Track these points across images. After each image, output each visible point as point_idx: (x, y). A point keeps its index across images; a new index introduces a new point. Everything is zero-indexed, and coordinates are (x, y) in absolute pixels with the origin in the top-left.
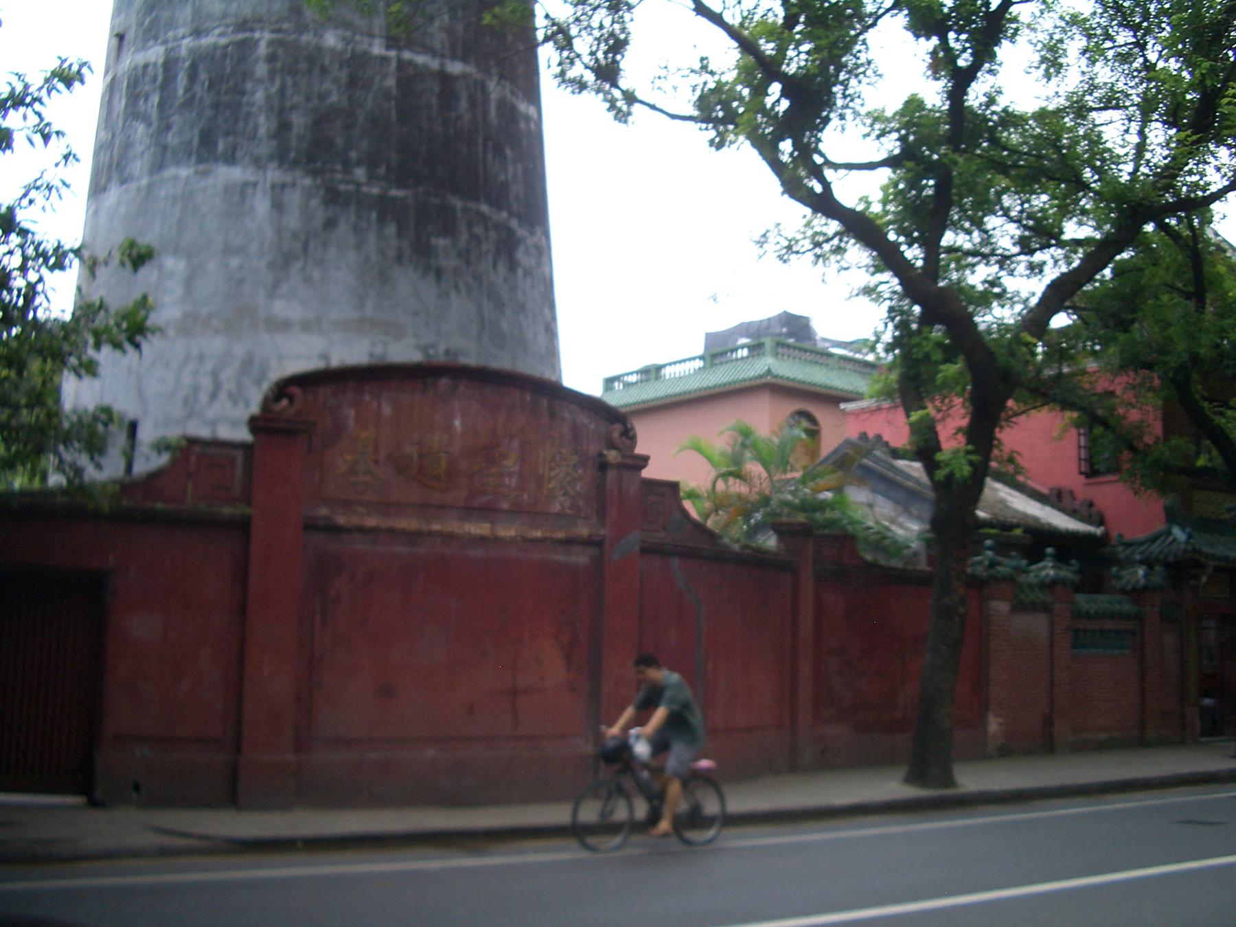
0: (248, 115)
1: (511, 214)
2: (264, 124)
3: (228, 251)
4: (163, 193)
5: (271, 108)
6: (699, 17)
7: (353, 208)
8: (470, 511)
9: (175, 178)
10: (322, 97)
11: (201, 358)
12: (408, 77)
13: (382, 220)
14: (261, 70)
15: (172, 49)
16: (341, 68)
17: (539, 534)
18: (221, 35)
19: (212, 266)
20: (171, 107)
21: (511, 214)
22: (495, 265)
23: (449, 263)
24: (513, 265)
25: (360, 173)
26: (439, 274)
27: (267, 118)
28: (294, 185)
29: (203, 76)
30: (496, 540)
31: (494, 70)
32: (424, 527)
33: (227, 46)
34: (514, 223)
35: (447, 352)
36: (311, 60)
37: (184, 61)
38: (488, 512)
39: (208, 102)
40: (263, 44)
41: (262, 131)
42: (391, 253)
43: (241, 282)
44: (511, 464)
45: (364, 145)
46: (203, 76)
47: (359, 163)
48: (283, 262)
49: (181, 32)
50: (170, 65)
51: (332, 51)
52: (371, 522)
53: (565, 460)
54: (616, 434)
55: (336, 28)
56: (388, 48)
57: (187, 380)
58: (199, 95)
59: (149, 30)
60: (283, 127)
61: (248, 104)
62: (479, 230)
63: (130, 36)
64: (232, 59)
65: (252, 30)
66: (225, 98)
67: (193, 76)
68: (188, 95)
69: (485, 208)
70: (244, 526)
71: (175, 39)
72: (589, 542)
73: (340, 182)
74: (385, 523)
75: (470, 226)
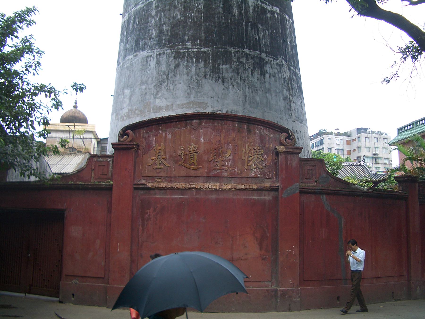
1: (261, 51)
2: (154, 32)
3: (142, 83)
4: (125, 66)
5: (157, 26)
8: (208, 178)
9: (129, 59)
10: (174, 18)
13: (198, 61)
14: (154, 13)
16: (181, 5)
17: (243, 187)
18: (142, 3)
19: (137, 90)
22: (252, 74)
23: (228, 75)
24: (263, 73)
25: (189, 44)
26: (223, 81)
27: (155, 30)
29: (137, 20)
30: (223, 190)
32: (187, 186)
33: (143, 7)
34: (264, 55)
35: (227, 112)
37: (132, 17)
38: (217, 178)
39: (138, 29)
41: (153, 35)
42: (202, 74)
43: (146, 94)
44: (229, 155)
45: (190, 33)
46: (137, 20)
48: (159, 84)
52: (162, 185)
53: (256, 152)
54: (283, 138)
60: (161, 32)
62: (244, 60)
66: (142, 26)
67: (134, 22)
68: (133, 28)
69: (247, 51)
70: (109, 189)
71: (131, 10)
72: (270, 189)
73: (181, 49)
74: (169, 185)
75: (239, 58)
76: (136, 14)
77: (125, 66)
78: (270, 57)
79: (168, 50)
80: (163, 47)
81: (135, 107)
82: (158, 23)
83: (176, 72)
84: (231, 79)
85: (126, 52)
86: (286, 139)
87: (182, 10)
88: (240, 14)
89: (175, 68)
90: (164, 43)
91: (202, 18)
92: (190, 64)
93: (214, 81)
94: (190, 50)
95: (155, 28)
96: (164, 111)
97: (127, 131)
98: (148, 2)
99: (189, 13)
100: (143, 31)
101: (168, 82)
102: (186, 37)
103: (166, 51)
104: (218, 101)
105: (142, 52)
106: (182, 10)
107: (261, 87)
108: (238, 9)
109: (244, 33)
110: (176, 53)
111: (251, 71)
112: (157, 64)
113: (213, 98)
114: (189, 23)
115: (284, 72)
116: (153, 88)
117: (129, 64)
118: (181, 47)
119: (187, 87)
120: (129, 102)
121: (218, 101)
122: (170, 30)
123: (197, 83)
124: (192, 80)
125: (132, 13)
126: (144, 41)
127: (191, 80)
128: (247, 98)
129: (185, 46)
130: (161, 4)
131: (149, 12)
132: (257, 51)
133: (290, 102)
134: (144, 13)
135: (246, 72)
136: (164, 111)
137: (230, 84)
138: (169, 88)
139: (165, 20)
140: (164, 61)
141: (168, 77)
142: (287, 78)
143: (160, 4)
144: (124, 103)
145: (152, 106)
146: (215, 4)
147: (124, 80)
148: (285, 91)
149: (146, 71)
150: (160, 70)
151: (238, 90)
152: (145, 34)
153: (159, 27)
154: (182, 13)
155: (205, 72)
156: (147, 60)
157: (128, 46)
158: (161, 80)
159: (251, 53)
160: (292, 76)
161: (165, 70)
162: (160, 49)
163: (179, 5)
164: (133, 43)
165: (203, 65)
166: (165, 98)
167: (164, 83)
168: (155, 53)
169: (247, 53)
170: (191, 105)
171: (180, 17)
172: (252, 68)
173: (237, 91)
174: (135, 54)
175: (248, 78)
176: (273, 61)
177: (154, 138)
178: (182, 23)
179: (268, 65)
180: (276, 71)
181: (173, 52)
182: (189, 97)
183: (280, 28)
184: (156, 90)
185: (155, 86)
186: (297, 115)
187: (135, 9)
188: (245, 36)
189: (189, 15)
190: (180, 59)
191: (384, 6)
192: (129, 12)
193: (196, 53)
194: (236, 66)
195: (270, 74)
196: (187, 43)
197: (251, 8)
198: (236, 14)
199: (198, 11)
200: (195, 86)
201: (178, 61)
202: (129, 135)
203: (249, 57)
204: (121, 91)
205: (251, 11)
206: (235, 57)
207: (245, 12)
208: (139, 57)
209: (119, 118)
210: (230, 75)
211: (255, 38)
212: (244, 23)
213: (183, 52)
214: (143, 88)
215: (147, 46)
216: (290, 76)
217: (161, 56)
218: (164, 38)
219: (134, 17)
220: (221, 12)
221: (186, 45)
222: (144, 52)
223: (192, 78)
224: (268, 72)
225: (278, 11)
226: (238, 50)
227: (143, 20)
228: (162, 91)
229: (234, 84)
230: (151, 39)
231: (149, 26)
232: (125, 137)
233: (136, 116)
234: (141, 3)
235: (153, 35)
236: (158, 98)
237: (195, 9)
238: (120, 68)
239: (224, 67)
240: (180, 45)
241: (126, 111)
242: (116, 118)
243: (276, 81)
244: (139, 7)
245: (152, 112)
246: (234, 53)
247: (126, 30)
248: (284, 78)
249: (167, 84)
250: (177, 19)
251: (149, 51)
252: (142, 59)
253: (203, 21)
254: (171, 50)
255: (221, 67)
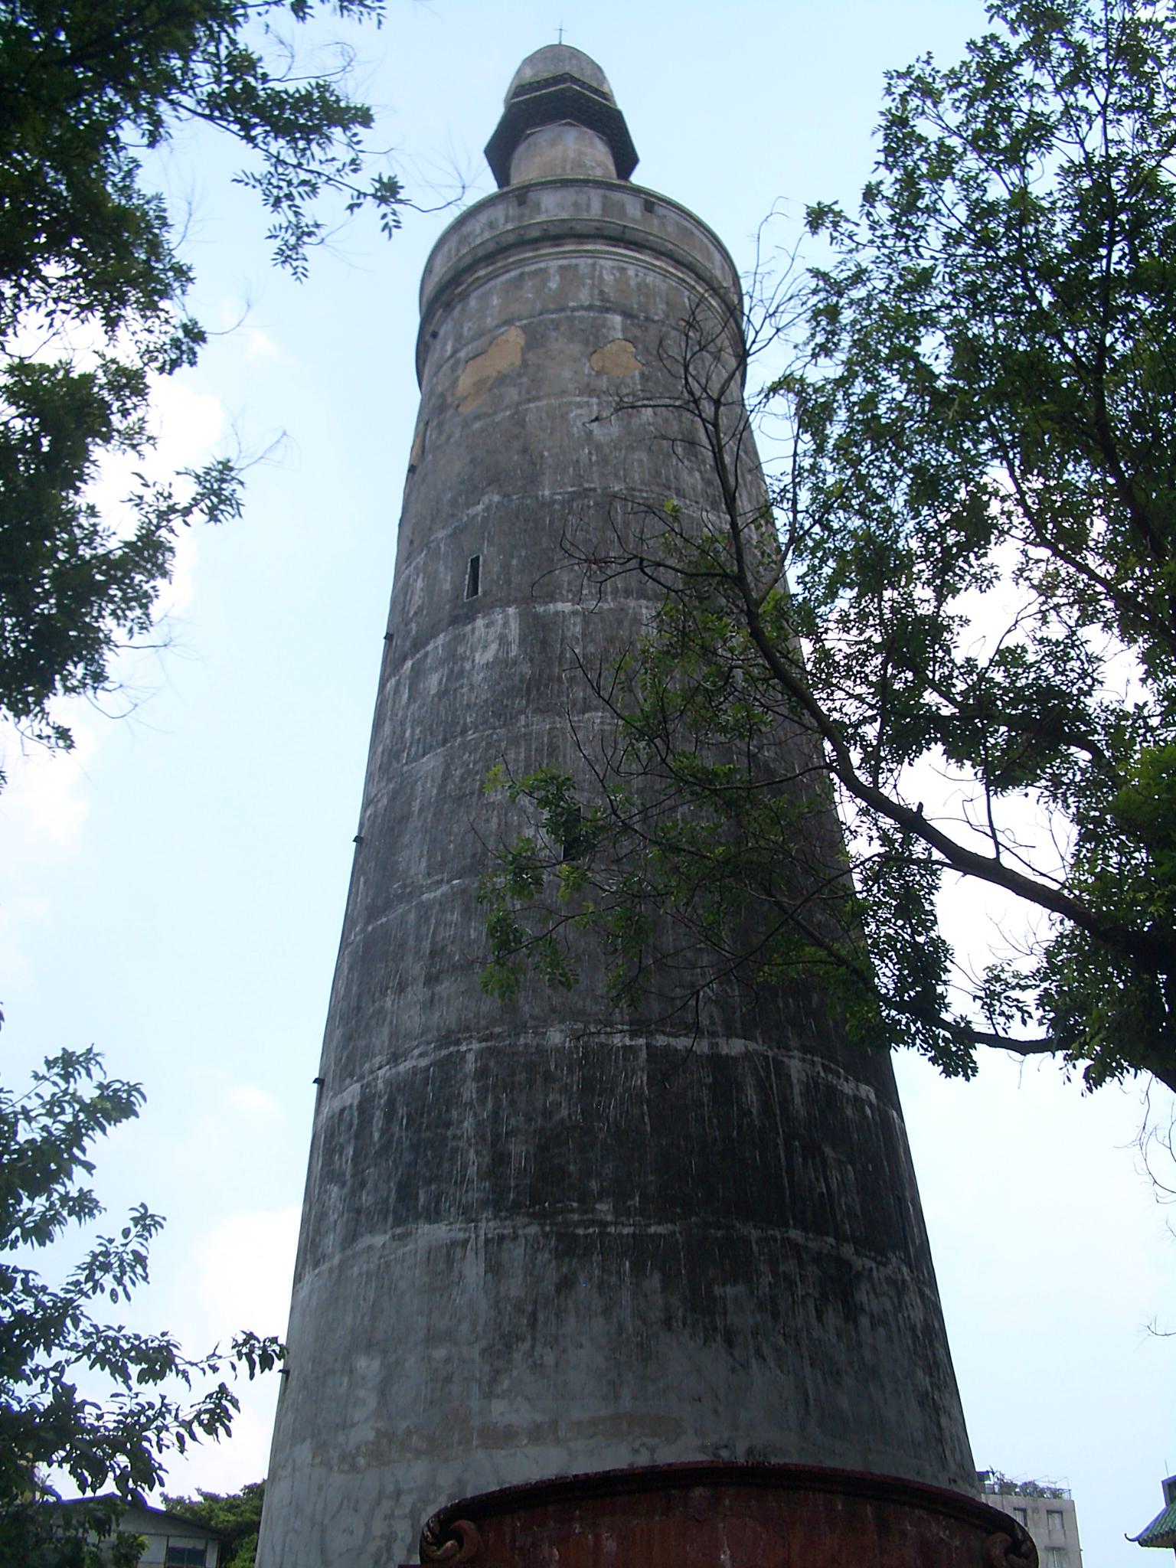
0: (455, 1150)
1: (840, 1238)
2: (474, 1161)
3: (432, 1338)
4: (356, 1271)
5: (483, 1137)
6: (969, 877)
7: (596, 1258)
9: (370, 1247)
10: (547, 1114)
11: (398, 1493)
12: (664, 1065)
13: (638, 1269)
14: (469, 1091)
15: (368, 1085)
16: (571, 1072)
18: (421, 1055)
19: (411, 1362)
20: (366, 1157)
21: (840, 1238)
24: (851, 1312)
25: (604, 1208)
27: (477, 1153)
28: (515, 1237)
29: (402, 1111)
31: (794, 1043)
33: (427, 1068)
34: (848, 1251)
35: (750, 1451)
36: (530, 1068)
37: (380, 1097)
39: (406, 1143)
40: (471, 1057)
41: (472, 1171)
43: (448, 1379)
45: (608, 1169)
46: (402, 1111)
47: (601, 1196)
49: (377, 1060)
50: (365, 1104)
51: (559, 1050)
54: (997, 1552)
55: (562, 1022)
56: (633, 1035)
57: (379, 1528)
58: (397, 1135)
59: (346, 1066)
60: (500, 1159)
61: (454, 1137)
62: (789, 1266)
63: (329, 1080)
64: (433, 1084)
65: (458, 1043)
67: (390, 1116)
69: (796, 1235)
71: (372, 1072)
73: (577, 1224)
76: (399, 1089)
77: (356, 1271)
78: (866, 1257)
79: (530, 1224)
80: (511, 1215)
81: (404, 1425)
82: (488, 1130)
83: (563, 1307)
84: (755, 1334)
85: (357, 1221)
86: (1007, 1552)
87: (575, 1088)
88: (766, 1108)
89: (558, 1290)
90: (514, 1200)
91: (646, 1119)
92: (613, 1279)
93: (700, 1342)
94: (609, 1230)
95: (477, 1144)
96: (526, 1445)
97: (457, 1523)
98: (444, 1052)
99: (600, 1102)
100: (429, 1153)
101: (534, 1339)
102: (594, 1183)
103: (524, 1227)
104: (716, 1411)
105: (427, 1227)
106: (575, 1088)
107: (851, 1363)
108: (757, 1094)
109: (784, 1174)
110: (561, 1236)
111: (816, 1306)
112: (489, 1276)
113: (700, 1400)
114: (601, 1136)
115: (910, 1308)
116: (477, 1358)
117: (372, 1266)
118: (576, 1217)
119: (607, 1359)
120: (379, 1403)
121: (716, 1411)
122: (535, 1156)
123: (640, 1345)
124: (624, 1335)
125: (380, 1085)
126: (433, 1187)
127: (620, 1335)
128: (812, 1401)
129: (591, 1216)
130: (497, 1062)
131: (451, 1086)
132: (827, 1234)
133: (936, 1408)
134: (433, 1091)
135: (801, 1310)
136: (526, 1445)
137: (752, 1351)
138: (539, 1362)
139: (513, 1121)
140: (516, 1264)
141: (535, 1319)
142: (919, 1326)
143: (492, 1063)
144: (354, 1405)
145: (476, 1423)
146: (685, 1072)
147: (349, 1320)
148: (920, 1373)
149: (446, 1295)
150: (502, 1293)
151: (778, 1372)
152: (440, 1164)
153: (494, 1144)
154: (574, 1100)
155: (667, 1308)
156: (448, 1255)
157: (364, 1198)
158: (509, 1332)
159: (810, 1244)
160: (930, 1322)
161: (523, 1296)
162: (501, 1220)
163: (562, 1070)
164: (389, 1192)
165: (658, 1285)
166: (527, 1398)
167: (520, 1343)
168: (482, 1232)
169: (797, 1245)
170: (625, 1426)
171: (569, 1114)
172: (817, 1295)
173: (777, 1375)
174: (398, 1231)
175: (807, 1330)
176: (878, 1269)
177: (556, 1552)
178: (576, 1135)
179: (865, 1286)
180: (888, 1306)
181: (548, 1234)
182: (617, 1398)
183: (884, 1158)
184: (492, 1365)
185: (484, 1350)
186: (958, 1456)
187: (393, 1070)
188: (787, 1185)
189: (599, 1104)
190: (575, 1261)
191: (366, 3)
192: (362, 1077)
193: (631, 1241)
194: (767, 1289)
195: (872, 1316)
196: (598, 1206)
197: (797, 1089)
198: (754, 1111)
199: (631, 1095)
200: (634, 1357)
201: (570, 1265)
202: (465, 1538)
203: (804, 1256)
204: (336, 1360)
205: (798, 1100)
206: (762, 1258)
207: (779, 1103)
208: (416, 1241)
209: (335, 1461)
210: (751, 1321)
211: (818, 1190)
212: (780, 1141)
213: (586, 1236)
214: (438, 1357)
215: (450, 1207)
216: (925, 1319)
217: (504, 1246)
218: (513, 1184)
219: (389, 1099)
220: (705, 1100)
221: (594, 1210)
222: (436, 1225)
223: (621, 1328)
224: (867, 1309)
225: (872, 1097)
226: (771, 1232)
227: (429, 1114)
228: (515, 1373)
229: (766, 1350)
230: (462, 1182)
231: (454, 1137)
232: (449, 1544)
233: (408, 1455)
234: (416, 1052)
235: (472, 1171)
236: (498, 1397)
237: (620, 1090)
238: (326, 1275)
239: (730, 1290)
240: (572, 1211)
241: (363, 1433)
242: (318, 1460)
243: (890, 1339)
244: (404, 1067)
245: (477, 1447)
246: (757, 1243)
247: (353, 1141)
248: (913, 1328)
249: (533, 1347)
250: (557, 1118)
251: (458, 1226)
252: (429, 1252)
253: (649, 1129)
254: (542, 1226)
255: (717, 1290)
